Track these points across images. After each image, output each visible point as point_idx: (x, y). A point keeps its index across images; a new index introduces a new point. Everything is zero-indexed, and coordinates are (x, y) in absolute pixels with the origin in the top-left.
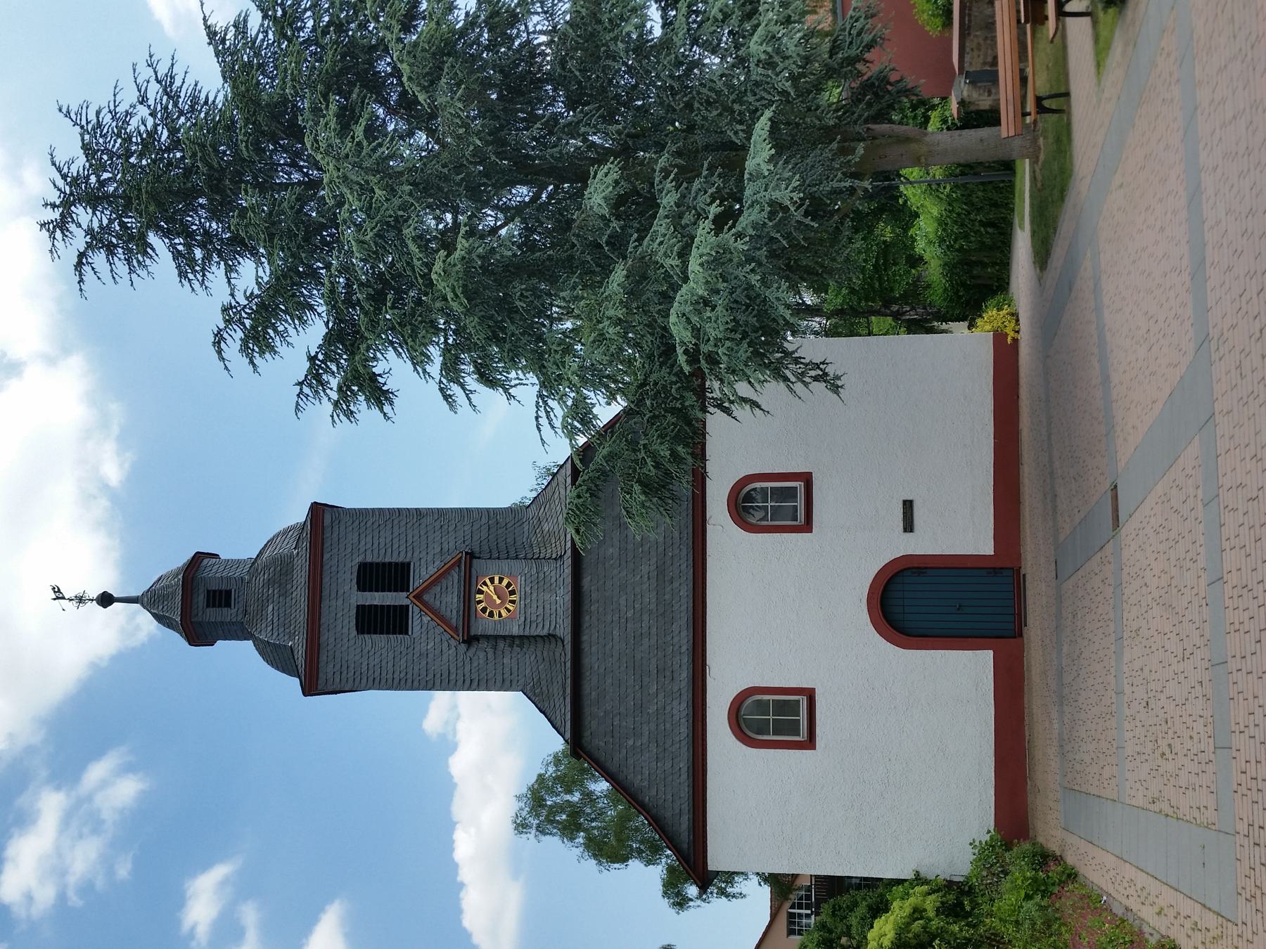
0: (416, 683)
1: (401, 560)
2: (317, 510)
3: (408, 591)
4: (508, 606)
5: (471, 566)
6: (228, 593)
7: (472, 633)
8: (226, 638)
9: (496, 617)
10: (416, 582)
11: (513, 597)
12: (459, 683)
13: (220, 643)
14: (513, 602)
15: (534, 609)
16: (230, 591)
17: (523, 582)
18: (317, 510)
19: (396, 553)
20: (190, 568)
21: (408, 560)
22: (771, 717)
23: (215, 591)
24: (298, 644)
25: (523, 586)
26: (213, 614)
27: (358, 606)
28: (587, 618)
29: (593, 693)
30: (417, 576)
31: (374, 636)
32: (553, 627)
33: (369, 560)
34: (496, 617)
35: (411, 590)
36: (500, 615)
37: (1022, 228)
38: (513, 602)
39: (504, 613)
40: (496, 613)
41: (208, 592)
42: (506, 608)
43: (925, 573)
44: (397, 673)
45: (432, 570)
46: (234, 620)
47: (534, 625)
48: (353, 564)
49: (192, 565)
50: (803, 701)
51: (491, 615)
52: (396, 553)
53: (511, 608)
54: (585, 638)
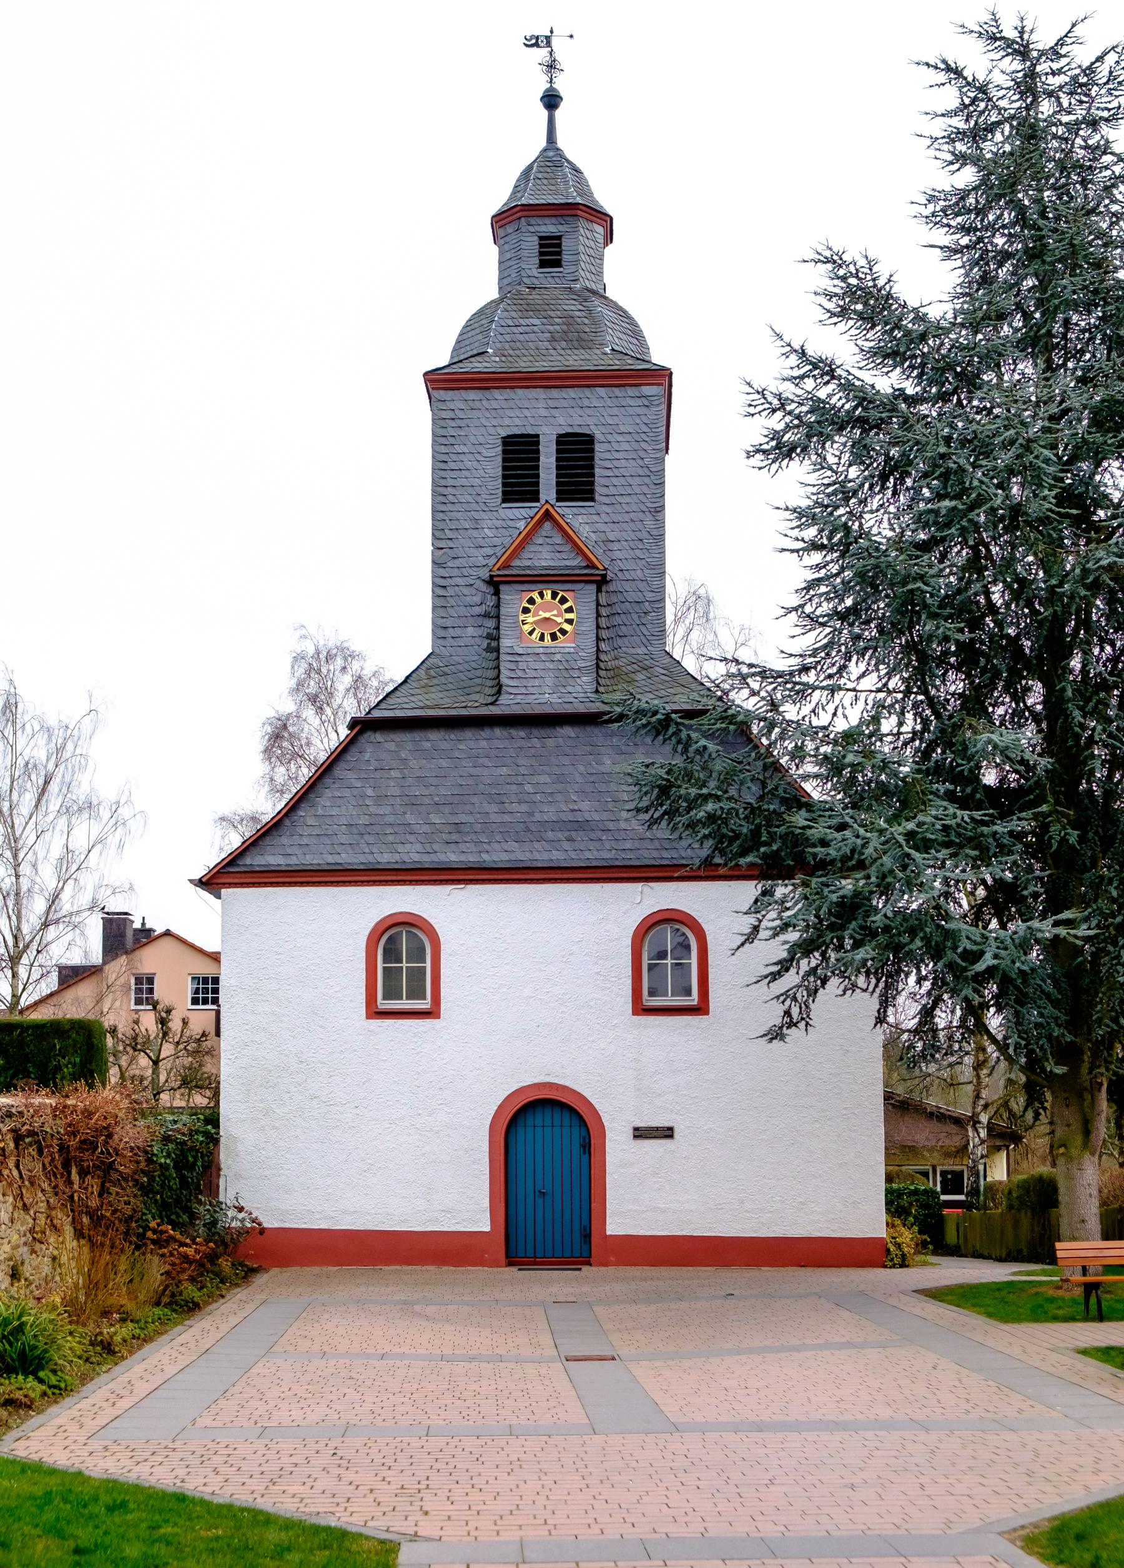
0: (441, 516)
4: (536, 632)
6: (558, 264)
11: (547, 638)
14: (542, 638)
16: (560, 266)
17: (567, 650)
22: (404, 965)
23: (559, 245)
27: (537, 436)
29: (429, 744)
30: (575, 510)
33: (598, 447)
38: (542, 638)
41: (559, 238)
42: (534, 630)
44: (453, 491)
48: (592, 427)
50: (425, 1004)
53: (534, 636)
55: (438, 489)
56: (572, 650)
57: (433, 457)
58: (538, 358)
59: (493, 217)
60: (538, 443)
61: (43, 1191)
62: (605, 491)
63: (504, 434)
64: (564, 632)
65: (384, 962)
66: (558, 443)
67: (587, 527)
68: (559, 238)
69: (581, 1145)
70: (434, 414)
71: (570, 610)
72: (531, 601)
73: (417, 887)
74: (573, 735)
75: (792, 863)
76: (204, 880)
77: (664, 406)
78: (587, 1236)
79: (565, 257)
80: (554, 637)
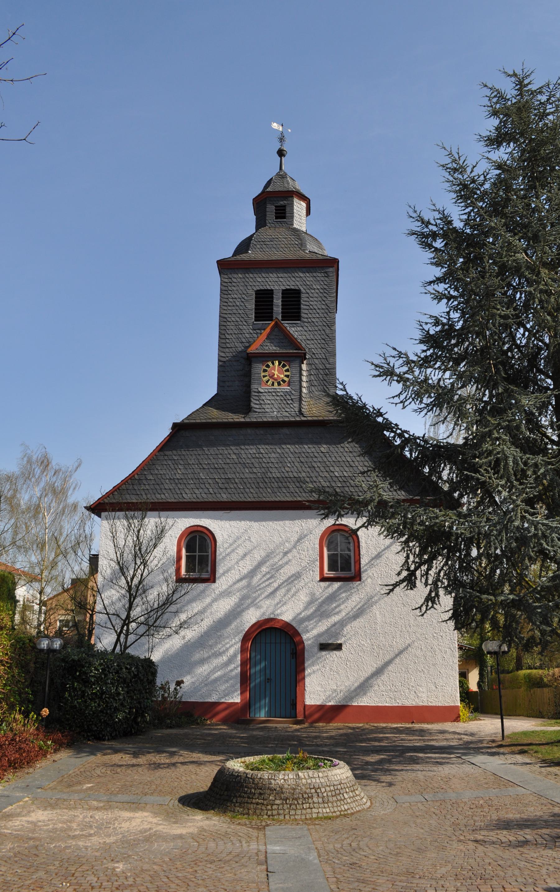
0: (223, 328)
1: (303, 315)
2: (333, 263)
3: (282, 320)
4: (270, 381)
5: (296, 357)
6: (284, 217)
7: (253, 359)
8: (256, 219)
9: (263, 374)
10: (286, 324)
11: (276, 384)
12: (223, 354)
13: (255, 217)
14: (273, 384)
15: (268, 398)
16: (285, 218)
17: (286, 390)
18: (333, 263)
19: (306, 311)
20: (356, 544)
21: (302, 319)
22: (197, 554)
23: (285, 210)
24: (251, 255)
25: (283, 390)
26: (271, 209)
27: (272, 290)
28: (262, 432)
29: (213, 437)
30: (291, 325)
31: (254, 301)
32: (255, 410)
33: (303, 295)
34: (263, 374)
35: (282, 322)
36: (264, 376)
37: (537, 726)
38: (273, 384)
39: (265, 379)
40: (266, 374)
41: (285, 206)
42: (269, 380)
43: (293, 658)
44: (230, 316)
45: (296, 335)
46: (267, 222)
47: (257, 398)
48: (300, 286)
49: (357, 548)
50: (205, 576)
51: (265, 371)
52: (306, 311)
53: (269, 383)
54: (249, 431)
55: (222, 315)
56: (288, 390)
57: (220, 300)
58: (271, 246)
59: (254, 199)
60: (272, 294)
61: (168, 585)
62: (305, 316)
63: (255, 289)
64: (284, 381)
65: (187, 552)
66: (282, 294)
67: (296, 333)
68: (285, 206)
69: (291, 654)
70: (221, 280)
71: (287, 371)
72: (268, 366)
73: (205, 512)
74: (288, 433)
75: (458, 493)
76: (92, 507)
77: (335, 277)
78: (294, 705)
79: (287, 215)
80: (279, 384)
